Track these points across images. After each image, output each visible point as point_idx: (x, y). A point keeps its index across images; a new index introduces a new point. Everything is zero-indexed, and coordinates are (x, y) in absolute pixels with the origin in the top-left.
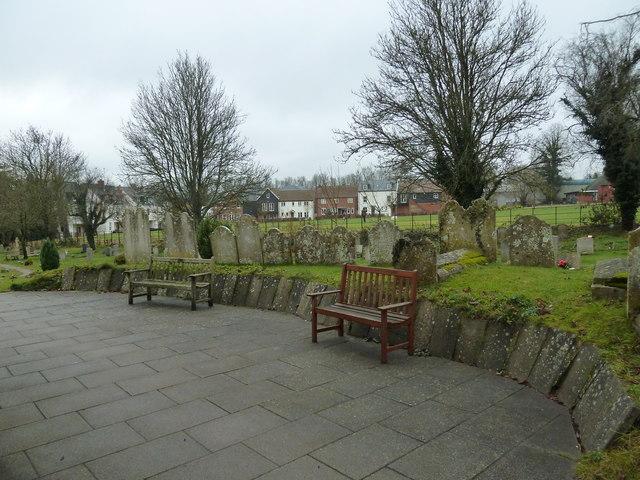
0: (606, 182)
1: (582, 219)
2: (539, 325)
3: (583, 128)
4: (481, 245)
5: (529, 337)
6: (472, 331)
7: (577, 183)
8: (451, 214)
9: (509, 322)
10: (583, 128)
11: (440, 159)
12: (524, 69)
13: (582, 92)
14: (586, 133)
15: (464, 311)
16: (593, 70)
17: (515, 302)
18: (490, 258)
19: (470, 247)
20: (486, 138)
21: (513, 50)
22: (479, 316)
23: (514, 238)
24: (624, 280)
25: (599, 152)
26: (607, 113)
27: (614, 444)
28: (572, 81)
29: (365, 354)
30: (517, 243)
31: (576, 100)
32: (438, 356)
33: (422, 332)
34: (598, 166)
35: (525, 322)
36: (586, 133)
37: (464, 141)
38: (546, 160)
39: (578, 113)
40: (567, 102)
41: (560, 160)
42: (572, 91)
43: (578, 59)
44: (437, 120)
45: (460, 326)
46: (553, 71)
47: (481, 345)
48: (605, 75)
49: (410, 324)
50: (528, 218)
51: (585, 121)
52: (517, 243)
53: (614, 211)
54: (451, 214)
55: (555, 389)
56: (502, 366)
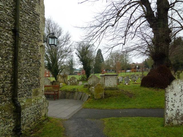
0: (83, 70)
1: (79, 78)
2: (77, 92)
3: (79, 59)
4: (65, 82)
5: (76, 94)
6: (68, 94)
7: (77, 70)
8: (59, 76)
9: (73, 92)
10: (79, 59)
11: (49, 64)
12: (68, 46)
13: (79, 52)
14: (80, 60)
15: (66, 91)
16: (81, 48)
17: (74, 89)
18: (67, 84)
19: (63, 83)
20: (59, 60)
21: (65, 41)
22: (69, 92)
23: (71, 81)
24: (87, 85)
25: (82, 64)
26: (84, 57)
27: (87, 100)
28: (77, 50)
29: (53, 100)
30: (71, 82)
31: (78, 53)
32: (63, 99)
33: (59, 95)
34: (82, 66)
35: (76, 91)
36: (80, 60)
37: (55, 60)
38: (69, 63)
39: (78, 56)
40: (76, 54)
41: (73, 64)
42: (77, 51)
43: (78, 45)
44: (49, 55)
45: (66, 94)
46: (73, 47)
47: (69, 96)
48: (83, 49)
49: (58, 94)
50: (73, 77)
51: (80, 58)
52: (71, 82)
53: (85, 76)
54: (59, 76)
55: (80, 99)
56: (73, 98)
